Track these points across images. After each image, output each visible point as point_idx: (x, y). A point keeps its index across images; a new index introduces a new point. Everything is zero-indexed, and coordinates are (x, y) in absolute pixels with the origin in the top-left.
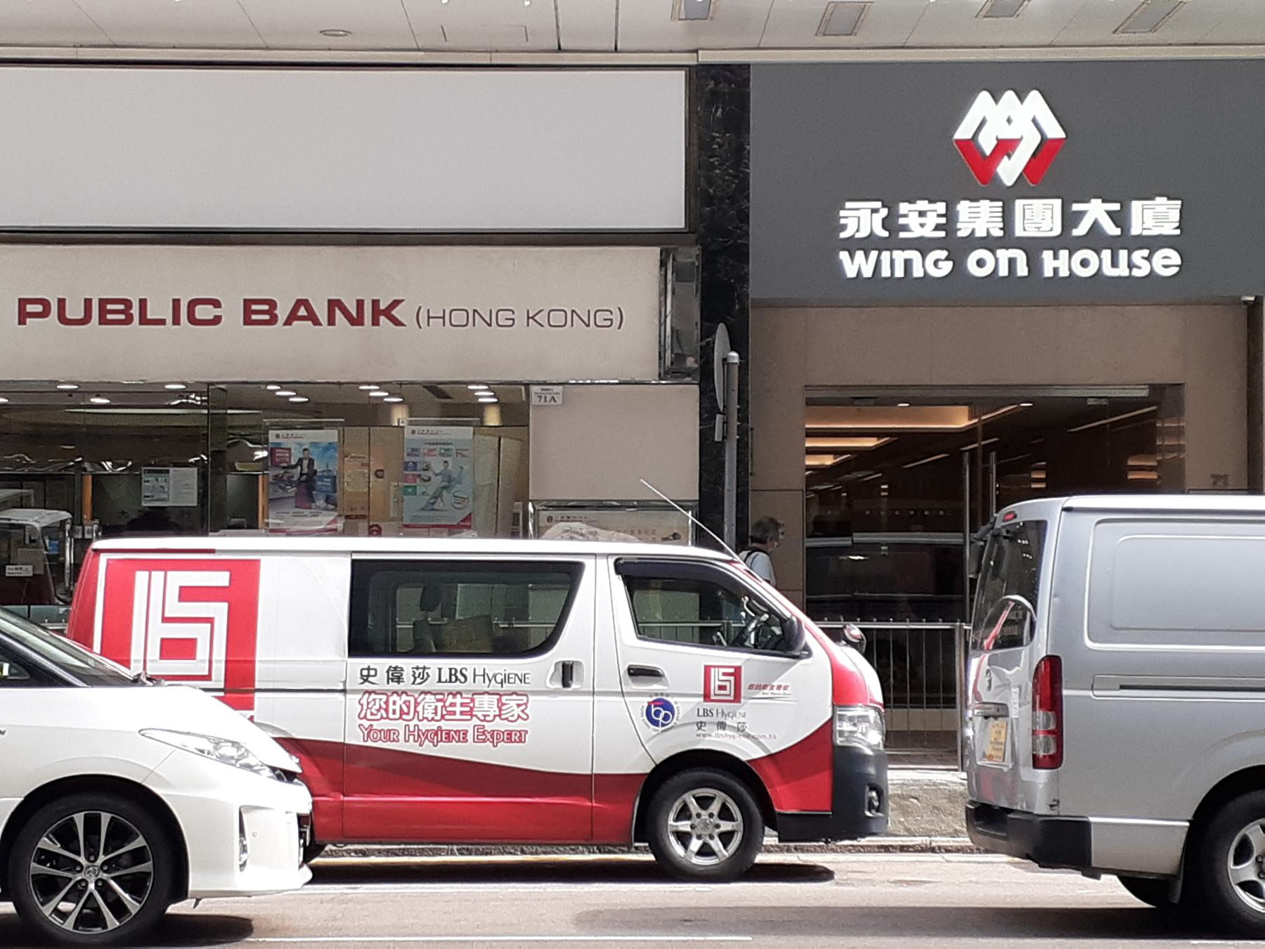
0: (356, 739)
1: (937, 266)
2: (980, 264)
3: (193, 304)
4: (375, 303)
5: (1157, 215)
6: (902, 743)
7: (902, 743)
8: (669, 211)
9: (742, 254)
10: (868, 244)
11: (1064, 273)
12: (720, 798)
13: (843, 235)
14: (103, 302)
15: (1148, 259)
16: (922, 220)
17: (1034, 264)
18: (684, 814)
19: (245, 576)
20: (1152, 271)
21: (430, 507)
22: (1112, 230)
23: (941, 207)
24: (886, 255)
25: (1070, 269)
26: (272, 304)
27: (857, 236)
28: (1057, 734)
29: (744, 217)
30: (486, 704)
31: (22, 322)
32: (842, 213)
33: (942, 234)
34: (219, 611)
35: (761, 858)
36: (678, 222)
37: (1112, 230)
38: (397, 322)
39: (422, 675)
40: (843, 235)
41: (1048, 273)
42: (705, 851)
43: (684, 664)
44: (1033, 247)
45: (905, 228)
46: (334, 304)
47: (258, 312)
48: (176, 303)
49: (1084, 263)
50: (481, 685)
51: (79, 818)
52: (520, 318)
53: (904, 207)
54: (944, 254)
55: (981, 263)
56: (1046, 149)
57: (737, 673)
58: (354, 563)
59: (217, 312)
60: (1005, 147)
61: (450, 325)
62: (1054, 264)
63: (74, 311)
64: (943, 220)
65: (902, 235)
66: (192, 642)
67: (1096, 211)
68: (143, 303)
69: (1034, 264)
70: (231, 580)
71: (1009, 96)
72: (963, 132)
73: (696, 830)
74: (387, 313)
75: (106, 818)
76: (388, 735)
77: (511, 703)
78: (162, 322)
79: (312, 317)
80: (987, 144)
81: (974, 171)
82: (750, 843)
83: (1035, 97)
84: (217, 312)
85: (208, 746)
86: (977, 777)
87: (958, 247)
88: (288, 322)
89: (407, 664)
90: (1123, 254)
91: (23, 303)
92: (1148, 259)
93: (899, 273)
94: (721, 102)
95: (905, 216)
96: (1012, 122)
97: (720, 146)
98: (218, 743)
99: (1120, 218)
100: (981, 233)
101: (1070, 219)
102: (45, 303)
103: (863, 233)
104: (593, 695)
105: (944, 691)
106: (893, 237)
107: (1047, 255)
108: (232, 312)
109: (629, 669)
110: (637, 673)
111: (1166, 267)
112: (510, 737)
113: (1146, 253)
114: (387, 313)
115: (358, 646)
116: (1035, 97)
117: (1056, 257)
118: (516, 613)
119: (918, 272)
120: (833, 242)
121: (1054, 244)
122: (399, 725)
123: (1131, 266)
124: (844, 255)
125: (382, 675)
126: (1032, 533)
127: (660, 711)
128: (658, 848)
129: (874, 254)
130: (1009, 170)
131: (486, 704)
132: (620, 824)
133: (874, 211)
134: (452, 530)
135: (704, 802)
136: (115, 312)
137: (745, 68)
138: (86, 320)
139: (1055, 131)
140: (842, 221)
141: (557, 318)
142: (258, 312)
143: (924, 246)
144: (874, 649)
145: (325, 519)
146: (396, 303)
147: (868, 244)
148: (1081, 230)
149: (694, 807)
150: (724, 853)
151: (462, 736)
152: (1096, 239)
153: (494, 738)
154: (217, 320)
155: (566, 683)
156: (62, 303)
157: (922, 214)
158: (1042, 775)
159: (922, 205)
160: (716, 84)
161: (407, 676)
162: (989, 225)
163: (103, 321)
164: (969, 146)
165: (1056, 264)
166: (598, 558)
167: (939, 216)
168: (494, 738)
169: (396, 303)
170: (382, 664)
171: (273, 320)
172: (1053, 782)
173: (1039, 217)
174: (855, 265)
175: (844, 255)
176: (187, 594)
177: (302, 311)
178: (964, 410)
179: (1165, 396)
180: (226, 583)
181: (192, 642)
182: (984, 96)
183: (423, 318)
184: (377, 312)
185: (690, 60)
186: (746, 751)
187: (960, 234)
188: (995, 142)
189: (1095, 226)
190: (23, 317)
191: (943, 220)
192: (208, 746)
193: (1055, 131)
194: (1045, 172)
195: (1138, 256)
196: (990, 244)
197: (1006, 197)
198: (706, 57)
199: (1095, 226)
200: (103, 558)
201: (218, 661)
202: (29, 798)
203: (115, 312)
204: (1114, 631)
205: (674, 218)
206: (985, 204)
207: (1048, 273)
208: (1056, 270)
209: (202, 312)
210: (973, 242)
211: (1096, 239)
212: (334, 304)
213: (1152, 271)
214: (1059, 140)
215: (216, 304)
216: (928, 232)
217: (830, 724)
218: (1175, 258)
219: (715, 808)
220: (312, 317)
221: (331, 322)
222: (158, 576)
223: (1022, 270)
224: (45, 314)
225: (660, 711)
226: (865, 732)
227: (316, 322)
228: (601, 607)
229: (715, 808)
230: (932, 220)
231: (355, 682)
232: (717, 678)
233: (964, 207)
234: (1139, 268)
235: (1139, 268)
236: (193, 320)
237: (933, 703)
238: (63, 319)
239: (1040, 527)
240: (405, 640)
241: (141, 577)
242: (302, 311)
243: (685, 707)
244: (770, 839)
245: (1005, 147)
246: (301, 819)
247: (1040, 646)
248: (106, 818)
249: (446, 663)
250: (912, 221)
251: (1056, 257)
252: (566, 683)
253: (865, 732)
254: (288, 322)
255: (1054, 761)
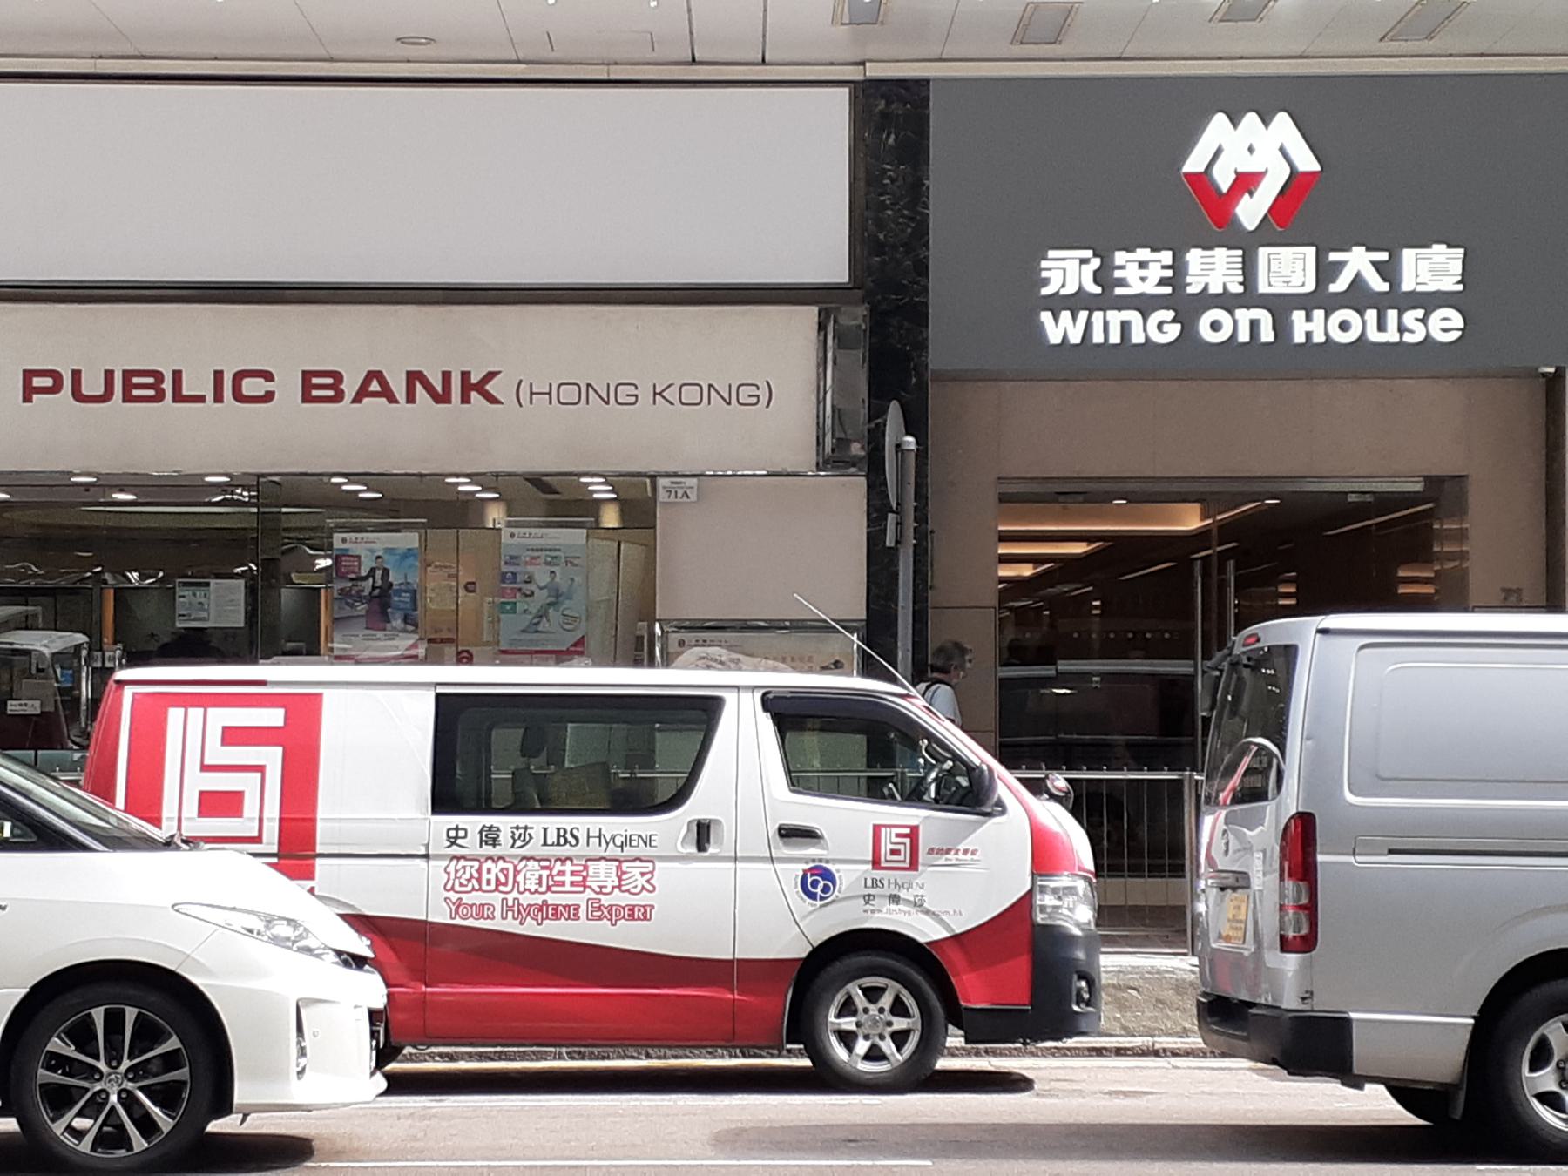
0: (441, 916)
1: (1162, 329)
2: (1215, 327)
3: (239, 376)
4: (465, 375)
5: (1434, 267)
6: (1118, 921)
7: (1118, 921)
8: (829, 262)
9: (919, 315)
10: (1076, 302)
11: (1319, 338)
12: (893, 988)
13: (1045, 291)
14: (128, 375)
15: (1424, 321)
16: (1143, 273)
17: (1282, 327)
18: (848, 1008)
19: (304, 714)
20: (1428, 335)
21: (533, 628)
22: (1379, 285)
23: (1166, 257)
24: (1098, 316)
25: (1326, 334)
26: (337, 376)
27: (1063, 292)
28: (1311, 909)
29: (922, 269)
30: (603, 873)
31: (27, 398)
32: (1044, 264)
33: (1168, 290)
34: (272, 757)
35: (943, 1063)
36: (841, 275)
37: (1379, 285)
38: (492, 399)
39: (523, 836)
40: (1045, 291)
41: (1299, 338)
42: (874, 1055)
43: (848, 823)
44: (1280, 306)
45: (1122, 283)
46: (414, 377)
47: (319, 387)
48: (219, 375)
49: (1344, 326)
50: (596, 849)
51: (98, 1014)
52: (645, 395)
53: (1120, 257)
54: (1170, 314)
55: (1215, 326)
56: (1297, 185)
57: (913, 834)
58: (439, 698)
59: (270, 386)
60: (1246, 182)
61: (558, 403)
62: (1306, 327)
63: (92, 386)
64: (1169, 273)
65: (1119, 291)
66: (238, 796)
67: (1358, 262)
68: (177, 375)
69: (1282, 327)
70: (286, 718)
71: (1251, 119)
72: (1194, 163)
73: (863, 1028)
74: (480, 387)
75: (131, 1014)
76: (481, 910)
77: (634, 871)
78: (200, 399)
79: (387, 393)
80: (1224, 179)
81: (1208, 212)
82: (930, 1044)
83: (1282, 120)
84: (270, 386)
85: (258, 925)
86: (1211, 962)
87: (1187, 307)
88: (357, 399)
89: (505, 823)
90: (1392, 315)
91: (28, 375)
92: (1424, 321)
93: (1115, 338)
94: (893, 126)
95: (1122, 267)
96: (1255, 151)
97: (893, 181)
98: (270, 921)
99: (1388, 271)
100: (1216, 289)
101: (1326, 272)
102: (56, 375)
103: (1070, 289)
104: (735, 861)
105: (1170, 856)
106: (1107, 294)
107: (1298, 316)
108: (288, 387)
109: (780, 829)
110: (789, 833)
111: (1445, 330)
112: (632, 913)
113: (1420, 313)
114: (480, 387)
115: (444, 800)
116: (1282, 120)
117: (1309, 319)
118: (639, 760)
119: (1137, 337)
120: (1032, 299)
121: (1307, 303)
122: (495, 899)
123: (1402, 329)
124: (1046, 317)
125: (474, 836)
126: (1279, 661)
127: (818, 881)
128: (816, 1051)
129: (1083, 315)
130: (1251, 211)
131: (603, 873)
132: (769, 1021)
133: (1084, 261)
134: (561, 657)
135: (872, 994)
136: (143, 386)
137: (923, 84)
138: (106, 396)
139: (1307, 162)
140: (1044, 274)
141: (690, 395)
142: (319, 387)
143: (1145, 305)
144: (1083, 804)
145: (403, 643)
146: (491, 375)
147: (1076, 302)
148: (1340, 285)
149: (860, 1000)
150: (897, 1057)
151: (572, 912)
152: (1358, 296)
153: (612, 914)
154: (268, 397)
155: (701, 847)
156: (76, 375)
157: (1143, 265)
158: (1292, 960)
159: (1143, 254)
160: (888, 104)
161: (505, 837)
162: (1226, 279)
163: (128, 398)
164: (1201, 181)
165: (1309, 327)
166: (742, 692)
167: (1164, 267)
168: (612, 914)
169: (491, 375)
170: (473, 823)
171: (338, 397)
172: (1305, 969)
173: (1287, 269)
174: (1060, 329)
175: (1046, 317)
176: (232, 736)
177: (375, 385)
178: (1195, 508)
179: (1444, 491)
180: (280, 722)
181: (238, 796)
182: (1220, 120)
183: (525, 394)
184: (467, 387)
185: (855, 74)
186: (925, 931)
187: (1190, 290)
188: (1233, 177)
189: (1358, 280)
190: (28, 393)
191: (1169, 273)
192: (258, 925)
193: (1307, 162)
194: (1295, 213)
195: (1411, 317)
196: (1227, 302)
197: (1248, 245)
198: (875, 71)
199: (1358, 280)
200: (128, 692)
201: (270, 820)
202: (36, 989)
203: (143, 386)
204: (1380, 782)
205: (836, 270)
206: (1221, 253)
207: (1299, 338)
208: (1308, 335)
209: (251, 387)
210: (1206, 300)
211: (1358, 296)
212: (414, 377)
213: (1428, 335)
214: (1313, 174)
215: (268, 376)
216: (1151, 288)
217: (1028, 897)
218: (1457, 320)
219: (886, 1001)
220: (387, 393)
221: (411, 398)
222: (196, 713)
223: (1267, 335)
224: (56, 389)
225: (818, 881)
226: (1072, 908)
227: (392, 399)
228: (745, 752)
229: (886, 1001)
230: (1155, 273)
231: (440, 846)
232: (888, 840)
233: (1194, 257)
234: (1412, 332)
235: (1412, 332)
236: (239, 397)
237: (1156, 871)
238: (78, 395)
239: (1289, 653)
240: (502, 794)
241: (175, 715)
242: (375, 385)
243: (849, 876)
244: (955, 1039)
245: (1246, 182)
246: (374, 1015)
247: (1289, 801)
248: (131, 1014)
249: (553, 822)
250: (1131, 273)
251: (1309, 319)
252: (701, 847)
253: (1072, 908)
254: (357, 399)
255: (1306, 943)
